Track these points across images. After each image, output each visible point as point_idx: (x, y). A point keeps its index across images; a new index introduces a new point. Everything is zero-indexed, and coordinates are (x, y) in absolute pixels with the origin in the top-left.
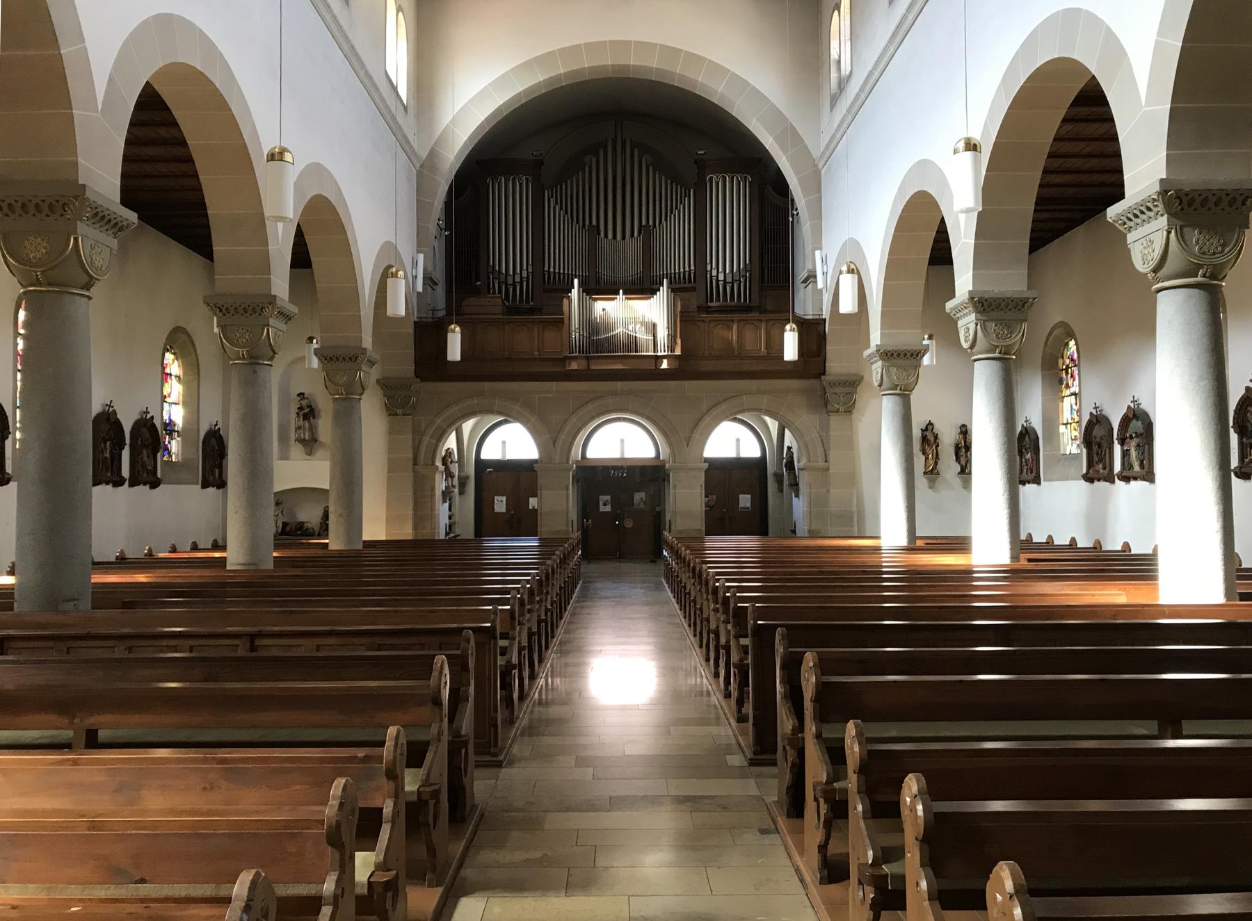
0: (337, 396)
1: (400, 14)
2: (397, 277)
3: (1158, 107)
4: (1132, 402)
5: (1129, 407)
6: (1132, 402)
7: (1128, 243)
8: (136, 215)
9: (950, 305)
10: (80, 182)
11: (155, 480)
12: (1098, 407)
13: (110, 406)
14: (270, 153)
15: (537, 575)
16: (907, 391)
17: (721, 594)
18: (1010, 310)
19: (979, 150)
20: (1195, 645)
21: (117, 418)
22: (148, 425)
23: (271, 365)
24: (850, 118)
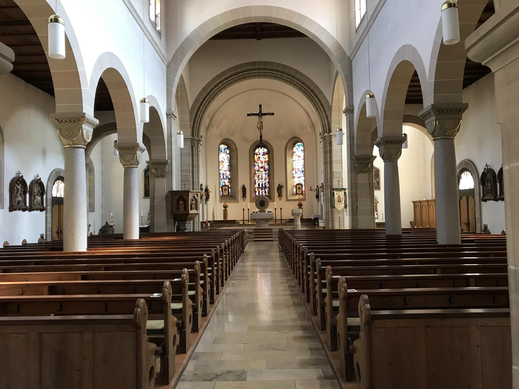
0: (126, 166)
2: (180, 134)
3: (194, 257)
4: (486, 166)
5: (485, 168)
6: (486, 166)
7: (425, 124)
8: (146, 147)
10: (84, 112)
11: (25, 208)
12: (488, 166)
13: (38, 176)
14: (141, 100)
16: (396, 159)
17: (292, 242)
18: (396, 144)
19: (374, 97)
21: (41, 181)
22: (20, 180)
23: (137, 167)
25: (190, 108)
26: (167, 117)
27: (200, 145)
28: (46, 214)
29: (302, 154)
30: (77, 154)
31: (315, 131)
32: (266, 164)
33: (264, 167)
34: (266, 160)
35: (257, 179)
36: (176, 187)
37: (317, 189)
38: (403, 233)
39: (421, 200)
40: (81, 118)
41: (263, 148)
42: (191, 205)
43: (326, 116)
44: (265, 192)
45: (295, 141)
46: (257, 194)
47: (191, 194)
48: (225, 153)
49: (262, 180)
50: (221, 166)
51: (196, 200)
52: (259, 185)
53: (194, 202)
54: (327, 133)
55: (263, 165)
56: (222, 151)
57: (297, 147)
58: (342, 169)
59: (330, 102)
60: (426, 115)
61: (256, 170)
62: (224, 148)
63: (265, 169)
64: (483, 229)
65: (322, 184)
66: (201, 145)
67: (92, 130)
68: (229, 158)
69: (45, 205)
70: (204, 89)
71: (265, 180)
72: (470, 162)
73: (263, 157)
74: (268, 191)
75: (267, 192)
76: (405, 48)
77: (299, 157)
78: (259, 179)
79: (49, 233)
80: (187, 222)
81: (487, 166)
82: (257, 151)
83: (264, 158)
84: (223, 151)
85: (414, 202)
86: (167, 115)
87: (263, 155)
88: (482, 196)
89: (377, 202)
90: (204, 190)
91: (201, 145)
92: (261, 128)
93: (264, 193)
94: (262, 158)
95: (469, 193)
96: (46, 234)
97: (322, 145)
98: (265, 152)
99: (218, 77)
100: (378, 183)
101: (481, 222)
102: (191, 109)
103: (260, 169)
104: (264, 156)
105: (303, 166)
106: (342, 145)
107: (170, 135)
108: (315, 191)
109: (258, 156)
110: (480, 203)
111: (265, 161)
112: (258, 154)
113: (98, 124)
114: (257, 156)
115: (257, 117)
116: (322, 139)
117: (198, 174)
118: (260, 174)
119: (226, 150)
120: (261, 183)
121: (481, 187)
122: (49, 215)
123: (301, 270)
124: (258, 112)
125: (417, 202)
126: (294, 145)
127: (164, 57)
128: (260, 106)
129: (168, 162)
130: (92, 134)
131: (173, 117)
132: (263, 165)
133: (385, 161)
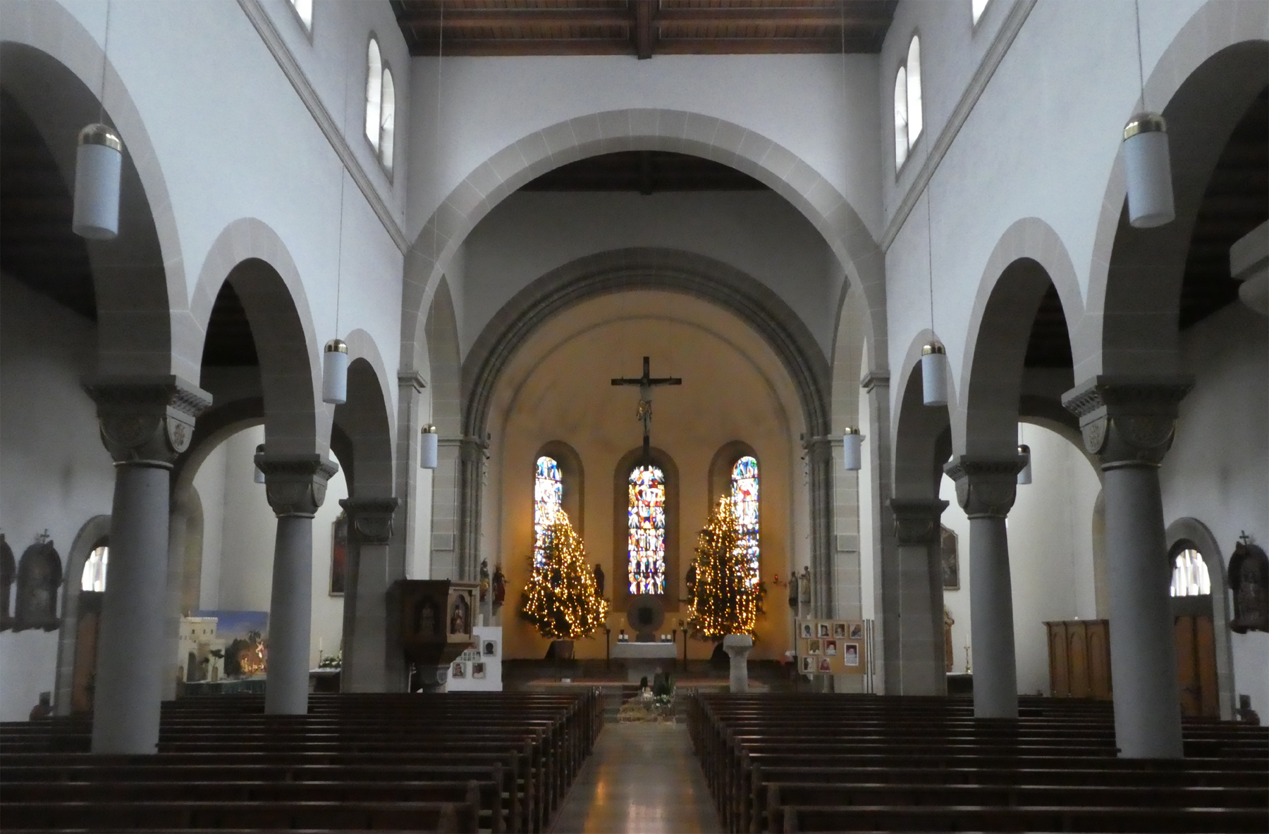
1: (387, 71)
2: (429, 432)
5: (1238, 545)
6: (1241, 537)
9: (1067, 398)
12: (1247, 537)
13: (46, 536)
15: (544, 732)
20: (1206, 806)
24: (937, 157)
25: (462, 361)
26: (399, 386)
27: (484, 457)
28: (62, 637)
29: (753, 488)
30: (148, 486)
31: (788, 429)
32: (660, 510)
33: (653, 518)
34: (658, 499)
35: (634, 550)
36: (419, 568)
37: (791, 581)
38: (1021, 713)
39: (1067, 619)
40: (166, 390)
41: (650, 467)
42: (453, 620)
43: (818, 391)
44: (655, 585)
45: (733, 452)
46: (633, 589)
47: (455, 590)
48: (551, 479)
49: (648, 552)
50: (538, 514)
51: (466, 604)
52: (638, 565)
53: (461, 612)
54: (818, 435)
55: (651, 512)
56: (542, 474)
57: (742, 467)
58: (859, 532)
59: (828, 356)
60: (1081, 402)
61: (631, 525)
62: (550, 466)
63: (654, 523)
64: (1238, 706)
65: (806, 568)
66: (488, 458)
67: (192, 421)
68: (560, 493)
69: (59, 614)
70: (502, 313)
71: (655, 552)
72: (1198, 525)
73: (652, 493)
74: (662, 582)
75: (659, 584)
76: (1021, 227)
77: (747, 493)
78: (640, 549)
79: (66, 691)
80: (439, 666)
81: (1244, 537)
82: (635, 475)
83: (654, 495)
84: (545, 474)
85: (1049, 625)
86: (400, 379)
87: (651, 487)
88: (1232, 617)
89: (949, 621)
90: (491, 577)
91: (488, 458)
92: (646, 417)
93: (650, 587)
94: (649, 494)
95: (1199, 605)
96: (57, 694)
97: (808, 467)
98: (656, 477)
99: (540, 282)
100: (954, 571)
101: (1232, 690)
102: (464, 364)
103: (642, 524)
104: (653, 490)
105: (756, 518)
106: (860, 471)
107: (406, 432)
108: (788, 585)
109: (638, 489)
110: (1229, 640)
111: (657, 502)
112: (639, 483)
113: (211, 405)
114: (634, 488)
115: (636, 389)
116: (807, 450)
117: (476, 534)
118: (643, 537)
119: (553, 470)
120: (644, 561)
121: (1231, 592)
122: (69, 642)
123: (742, 823)
124: (639, 375)
125: (1058, 624)
126: (732, 462)
127: (398, 231)
128: (646, 360)
129: (396, 503)
130: (194, 432)
131: (415, 384)
132: (651, 512)
133: (973, 516)
